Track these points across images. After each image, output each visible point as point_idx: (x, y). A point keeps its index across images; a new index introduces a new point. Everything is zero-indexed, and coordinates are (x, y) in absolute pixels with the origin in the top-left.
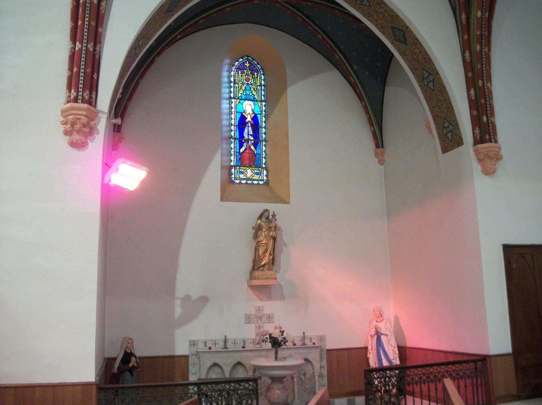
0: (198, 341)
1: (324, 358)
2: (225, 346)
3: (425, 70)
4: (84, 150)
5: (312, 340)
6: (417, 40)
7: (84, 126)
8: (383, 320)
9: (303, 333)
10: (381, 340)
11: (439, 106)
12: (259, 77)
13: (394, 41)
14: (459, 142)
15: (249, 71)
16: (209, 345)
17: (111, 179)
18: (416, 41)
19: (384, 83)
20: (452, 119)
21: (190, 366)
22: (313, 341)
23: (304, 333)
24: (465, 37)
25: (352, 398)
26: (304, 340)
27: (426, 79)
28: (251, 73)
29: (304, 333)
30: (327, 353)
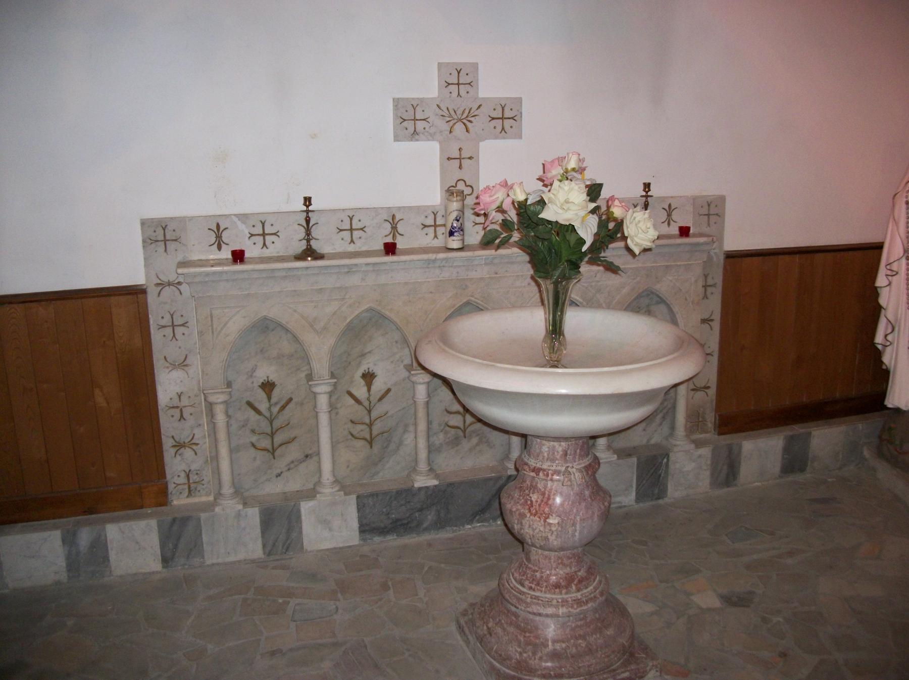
0: (182, 221)
2: (308, 241)
5: (675, 216)
9: (642, 187)
16: (237, 239)
17: (655, 317)
21: (156, 337)
23: (647, 186)
25: (798, 429)
29: (647, 186)
30: (725, 269)
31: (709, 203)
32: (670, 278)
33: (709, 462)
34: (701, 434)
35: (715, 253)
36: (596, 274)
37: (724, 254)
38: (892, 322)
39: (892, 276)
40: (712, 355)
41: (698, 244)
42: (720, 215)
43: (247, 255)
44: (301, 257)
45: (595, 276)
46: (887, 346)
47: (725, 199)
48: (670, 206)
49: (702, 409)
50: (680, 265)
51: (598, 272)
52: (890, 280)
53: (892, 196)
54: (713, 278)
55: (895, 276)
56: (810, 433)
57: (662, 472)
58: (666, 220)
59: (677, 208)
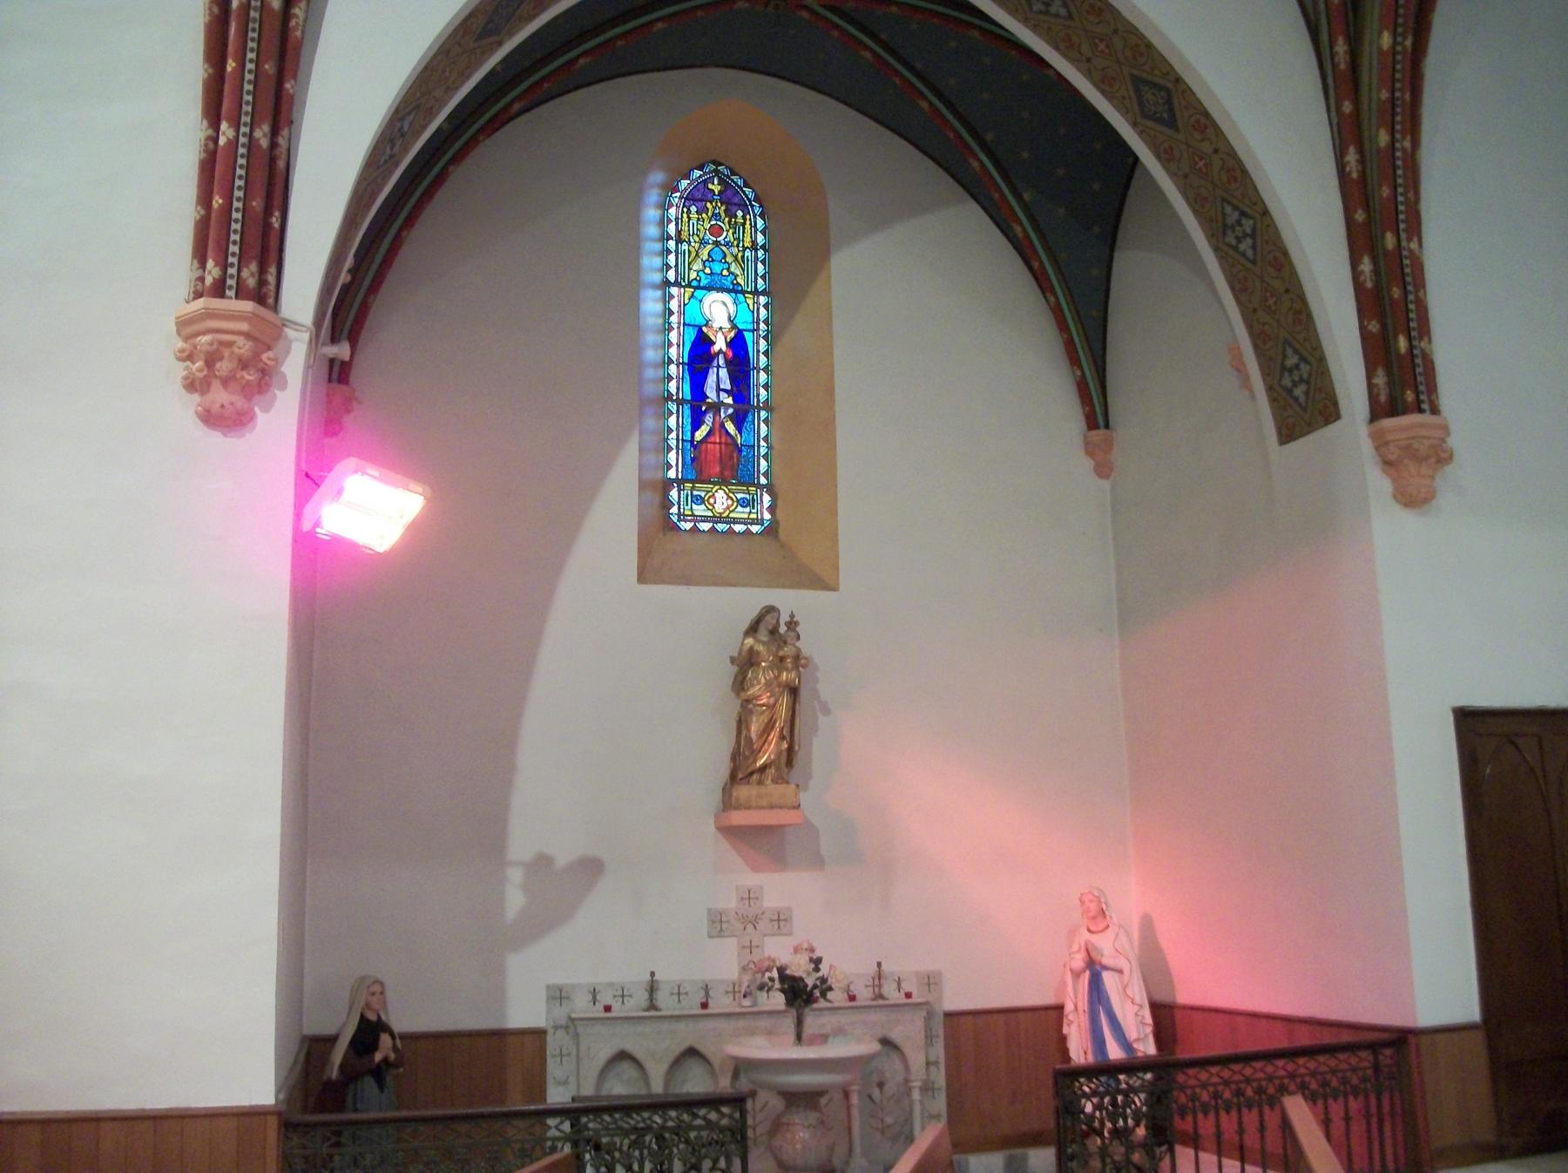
0: (573, 986)
1: (937, 1036)
2: (651, 1001)
3: (1229, 203)
4: (243, 436)
5: (903, 985)
6: (1207, 115)
7: (244, 364)
8: (1108, 926)
9: (876, 965)
10: (1103, 984)
11: (1270, 306)
12: (748, 222)
13: (1139, 120)
14: (1328, 411)
15: (719, 204)
16: (605, 998)
18: (1203, 120)
19: (1111, 240)
20: (1307, 344)
21: (550, 1061)
22: (906, 987)
23: (879, 965)
24: (1344, 108)
25: (1018, 1151)
26: (880, 986)
27: (1233, 227)
28: (725, 211)
29: (879, 965)
30: (945, 1024)
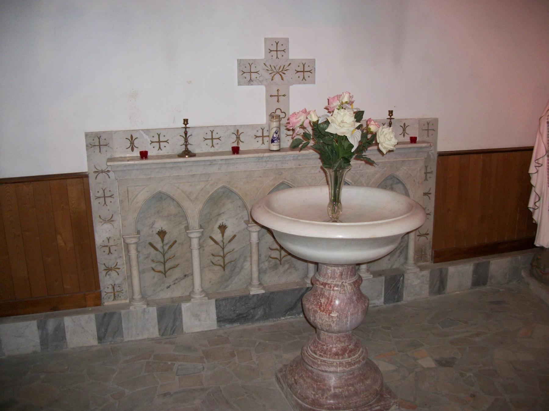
0: (110, 133)
2: (186, 146)
5: (407, 130)
9: (388, 113)
16: (143, 144)
21: (94, 204)
23: (391, 113)
25: (482, 259)
29: (391, 113)
30: (438, 162)
31: (428, 123)
32: (405, 168)
33: (428, 279)
34: (424, 262)
35: (432, 153)
36: (360, 166)
37: (437, 153)
38: (539, 195)
39: (539, 167)
40: (430, 215)
41: (421, 148)
42: (435, 130)
43: (149, 154)
44: (182, 155)
45: (360, 167)
46: (535, 209)
47: (438, 120)
48: (404, 124)
49: (424, 247)
50: (411, 160)
51: (361, 165)
52: (538, 169)
53: (539, 119)
54: (430, 168)
55: (541, 167)
56: (489, 262)
57: (400, 285)
58: (402, 133)
59: (409, 126)
